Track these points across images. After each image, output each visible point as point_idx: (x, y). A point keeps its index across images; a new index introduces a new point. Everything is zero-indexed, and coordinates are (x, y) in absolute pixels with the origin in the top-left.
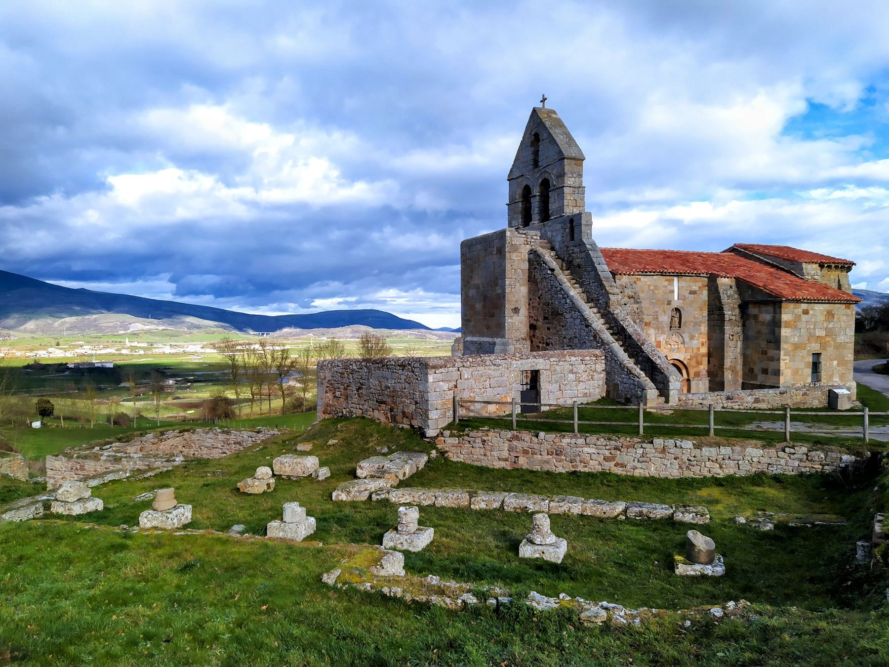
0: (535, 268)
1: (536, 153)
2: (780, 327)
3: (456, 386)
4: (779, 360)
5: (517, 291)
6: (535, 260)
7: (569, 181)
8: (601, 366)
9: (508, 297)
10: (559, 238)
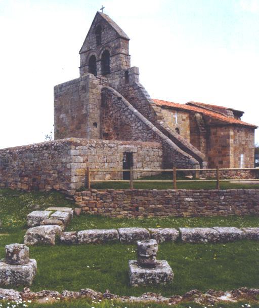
3: (87, 161)
4: (229, 155)
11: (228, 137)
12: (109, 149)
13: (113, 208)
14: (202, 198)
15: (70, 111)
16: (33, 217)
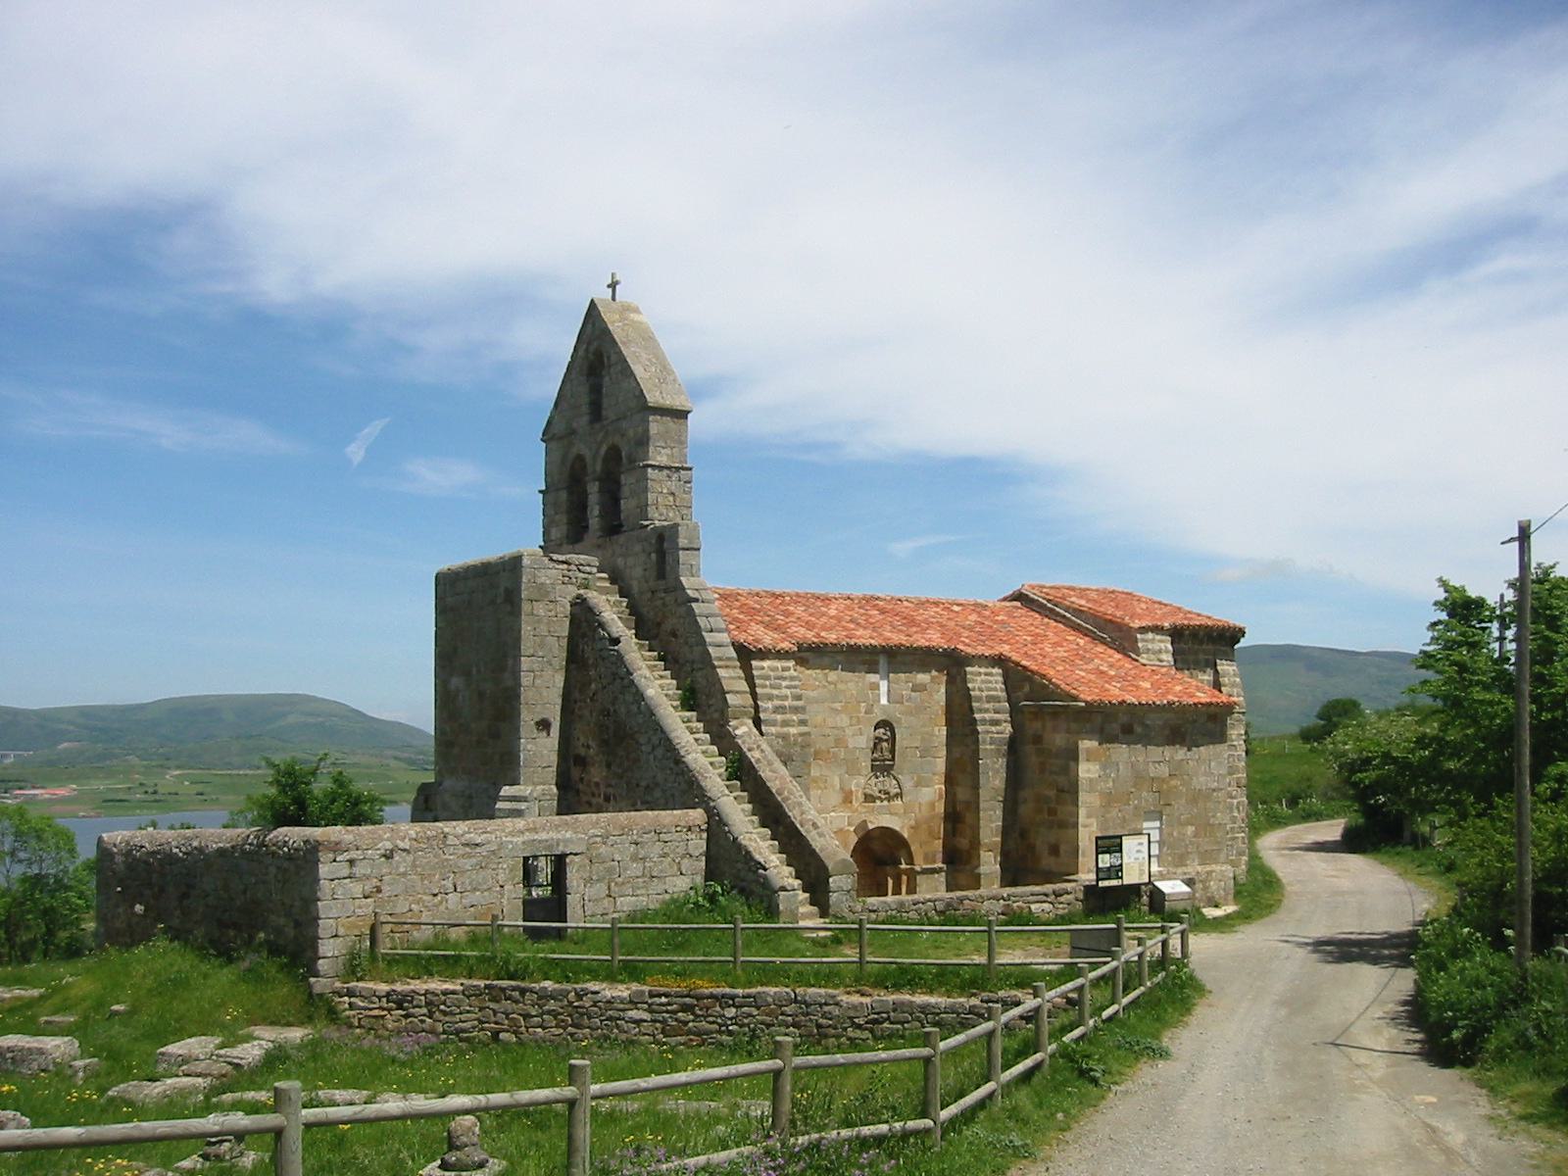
0: (584, 635)
1: (596, 391)
2: (1076, 759)
3: (379, 890)
4: (1076, 825)
5: (542, 685)
6: (583, 618)
7: (659, 456)
8: (698, 844)
9: (526, 695)
10: (638, 572)
11: (1073, 755)
12: (462, 850)
13: (431, 1033)
14: (674, 1012)
15: (474, 670)
16: (170, 1055)
